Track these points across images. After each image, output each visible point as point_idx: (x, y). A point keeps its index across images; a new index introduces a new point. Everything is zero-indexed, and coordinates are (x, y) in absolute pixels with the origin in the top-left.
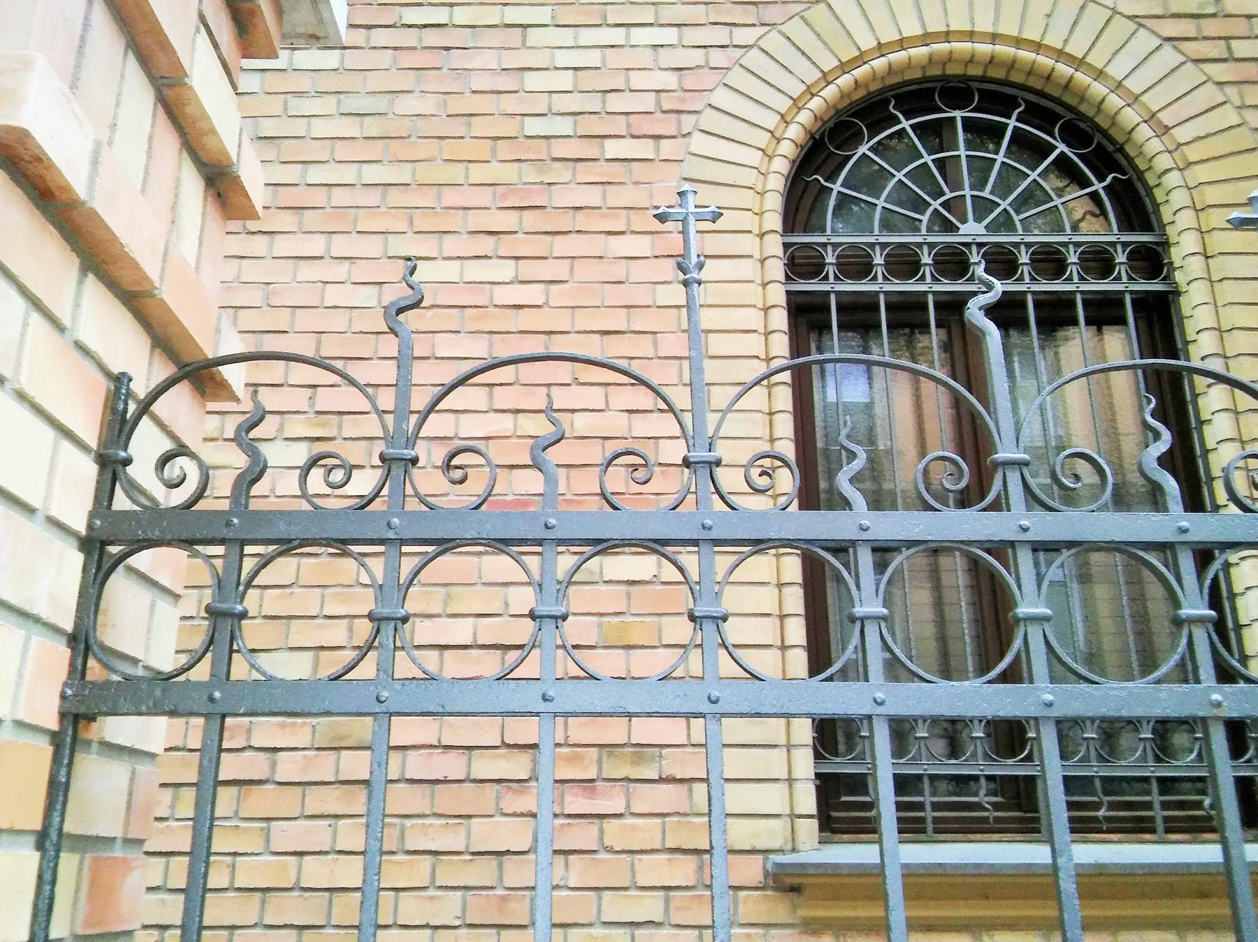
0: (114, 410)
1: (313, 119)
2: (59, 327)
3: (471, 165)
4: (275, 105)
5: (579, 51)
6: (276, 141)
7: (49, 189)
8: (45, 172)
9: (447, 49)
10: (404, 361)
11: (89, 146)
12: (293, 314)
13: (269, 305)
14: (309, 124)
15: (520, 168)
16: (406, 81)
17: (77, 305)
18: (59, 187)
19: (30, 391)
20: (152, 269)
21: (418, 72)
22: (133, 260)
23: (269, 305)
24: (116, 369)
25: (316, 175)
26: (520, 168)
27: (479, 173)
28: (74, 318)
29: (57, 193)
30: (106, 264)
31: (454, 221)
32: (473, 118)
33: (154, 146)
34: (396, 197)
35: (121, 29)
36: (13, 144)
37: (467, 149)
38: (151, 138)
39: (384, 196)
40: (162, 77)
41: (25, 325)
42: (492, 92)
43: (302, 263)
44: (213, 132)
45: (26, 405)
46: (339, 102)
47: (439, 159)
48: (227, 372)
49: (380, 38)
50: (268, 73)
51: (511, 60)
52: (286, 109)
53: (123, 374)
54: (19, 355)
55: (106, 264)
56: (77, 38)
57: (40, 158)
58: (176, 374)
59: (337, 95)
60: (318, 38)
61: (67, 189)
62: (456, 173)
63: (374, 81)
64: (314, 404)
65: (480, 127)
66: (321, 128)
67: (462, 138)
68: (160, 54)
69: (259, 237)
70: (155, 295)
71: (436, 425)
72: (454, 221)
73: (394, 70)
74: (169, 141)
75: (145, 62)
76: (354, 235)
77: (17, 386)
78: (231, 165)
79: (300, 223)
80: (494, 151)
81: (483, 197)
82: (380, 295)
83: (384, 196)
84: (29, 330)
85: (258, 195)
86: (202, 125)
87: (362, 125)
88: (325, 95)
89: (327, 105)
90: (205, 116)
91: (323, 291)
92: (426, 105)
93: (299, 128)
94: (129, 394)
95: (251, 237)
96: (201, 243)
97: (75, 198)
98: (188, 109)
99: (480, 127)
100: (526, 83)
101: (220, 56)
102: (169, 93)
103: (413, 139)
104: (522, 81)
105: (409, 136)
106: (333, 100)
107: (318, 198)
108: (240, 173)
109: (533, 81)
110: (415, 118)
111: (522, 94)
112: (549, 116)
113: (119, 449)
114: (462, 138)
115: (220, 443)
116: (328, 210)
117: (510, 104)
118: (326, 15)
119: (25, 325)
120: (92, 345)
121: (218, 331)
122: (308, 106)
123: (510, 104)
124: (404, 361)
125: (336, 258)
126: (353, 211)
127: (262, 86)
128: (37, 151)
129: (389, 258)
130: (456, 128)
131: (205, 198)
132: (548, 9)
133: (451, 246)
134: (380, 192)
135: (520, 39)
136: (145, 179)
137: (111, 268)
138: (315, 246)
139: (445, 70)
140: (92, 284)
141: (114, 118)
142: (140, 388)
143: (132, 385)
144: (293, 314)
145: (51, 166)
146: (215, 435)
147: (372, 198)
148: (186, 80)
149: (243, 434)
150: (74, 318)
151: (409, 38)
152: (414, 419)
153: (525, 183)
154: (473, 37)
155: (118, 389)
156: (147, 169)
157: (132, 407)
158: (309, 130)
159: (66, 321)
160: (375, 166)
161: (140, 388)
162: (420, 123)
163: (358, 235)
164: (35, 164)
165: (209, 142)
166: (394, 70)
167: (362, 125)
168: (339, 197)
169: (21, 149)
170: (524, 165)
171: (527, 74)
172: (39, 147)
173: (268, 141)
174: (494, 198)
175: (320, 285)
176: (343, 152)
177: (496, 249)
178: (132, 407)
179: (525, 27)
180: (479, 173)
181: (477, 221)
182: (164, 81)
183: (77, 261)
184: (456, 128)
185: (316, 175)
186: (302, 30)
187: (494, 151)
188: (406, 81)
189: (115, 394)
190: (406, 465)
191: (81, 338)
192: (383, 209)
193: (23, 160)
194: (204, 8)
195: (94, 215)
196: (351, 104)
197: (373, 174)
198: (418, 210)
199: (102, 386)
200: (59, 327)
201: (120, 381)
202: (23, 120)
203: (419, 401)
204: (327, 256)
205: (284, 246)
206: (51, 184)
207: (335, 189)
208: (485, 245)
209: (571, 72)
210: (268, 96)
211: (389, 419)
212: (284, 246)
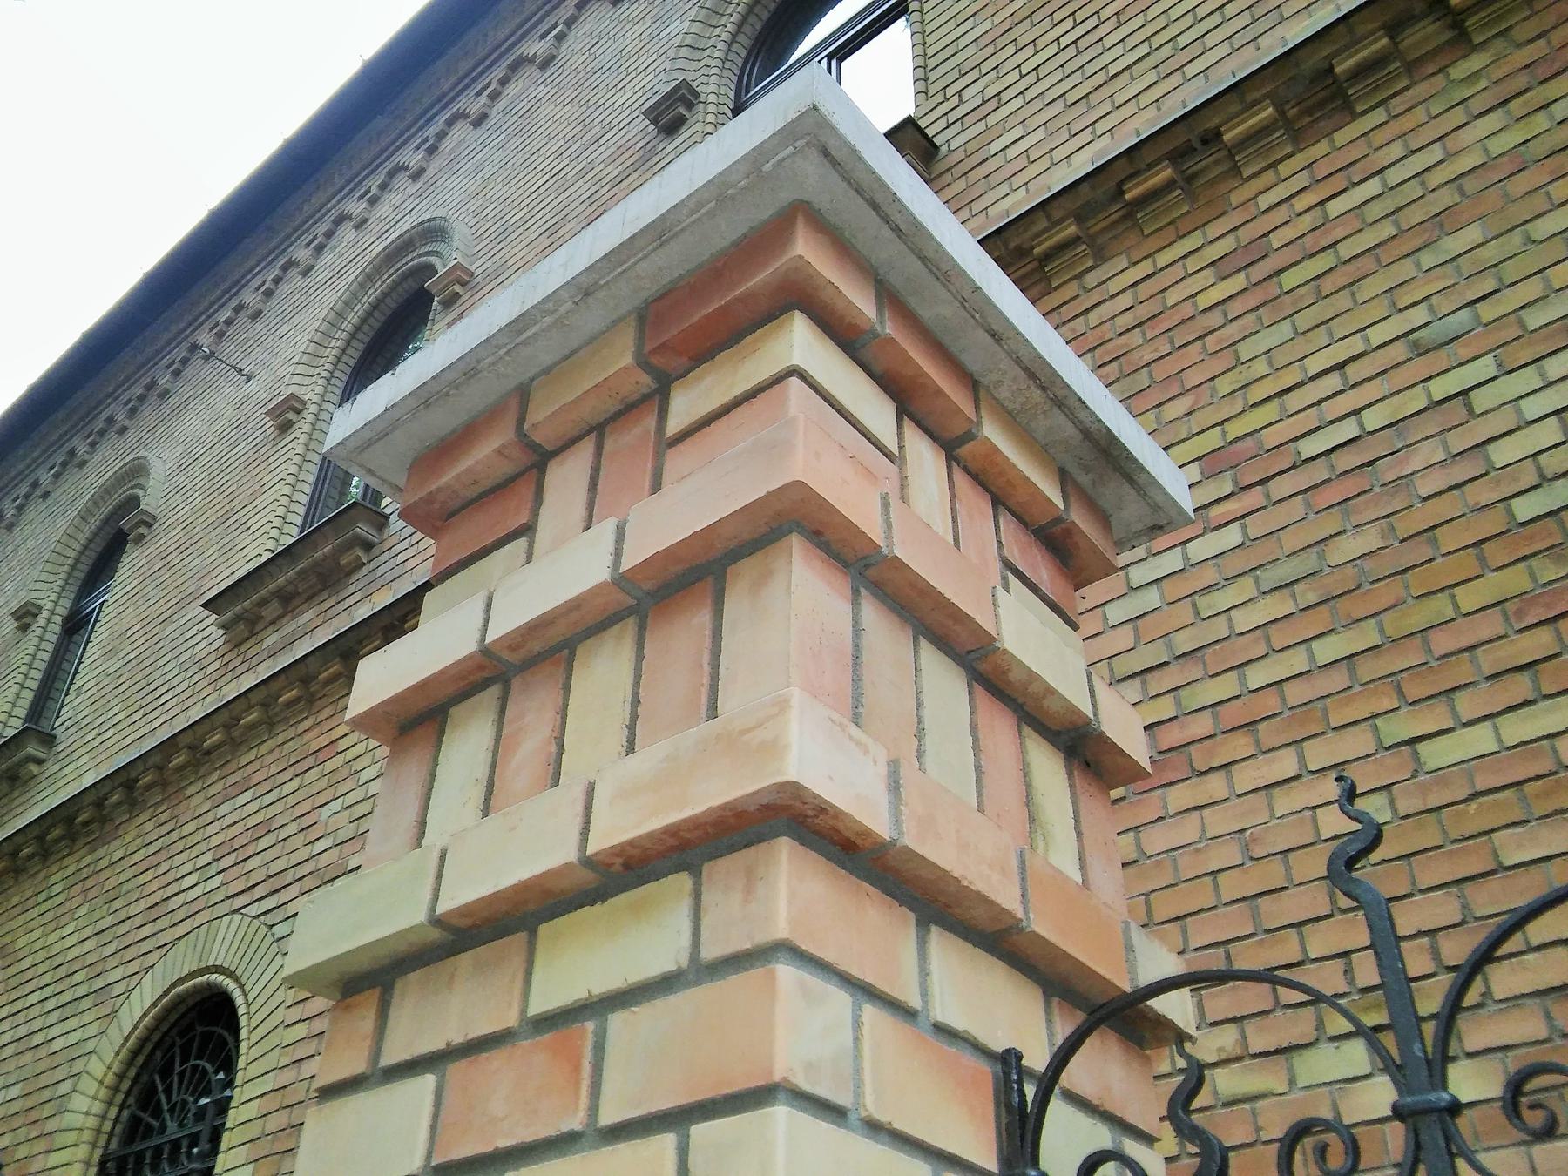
0: (1008, 1105)
1: (1233, 613)
2: (908, 1014)
3: (1456, 590)
4: (1184, 613)
5: (1555, 387)
6: (1199, 654)
7: (848, 840)
8: (835, 822)
9: (1371, 463)
10: (1386, 943)
11: (882, 770)
12: (1286, 862)
13: (1252, 859)
14: (1230, 620)
15: (1530, 567)
16: (1330, 524)
17: (924, 973)
18: (858, 834)
19: (883, 1117)
20: (1007, 897)
21: (1343, 506)
22: (978, 893)
23: (1252, 859)
24: (999, 1047)
25: (1257, 677)
26: (1530, 567)
27: (1469, 598)
28: (924, 993)
29: (859, 842)
30: (950, 907)
31: (1462, 671)
32: (1436, 531)
33: (981, 736)
34: (1369, 669)
35: (900, 616)
36: (790, 802)
37: (1445, 570)
38: (974, 729)
39: (1352, 672)
40: (969, 652)
41: (857, 1024)
42: (1451, 488)
43: (1276, 791)
44: (1051, 691)
45: (884, 1137)
46: (1257, 579)
47: (1410, 600)
48: (1161, 1004)
49: (1281, 487)
50: (1165, 581)
51: (1458, 442)
52: (1197, 613)
53: (1008, 1051)
54: (858, 1070)
55: (950, 907)
56: (849, 649)
57: (823, 808)
58: (1084, 1022)
59: (1252, 574)
60: (1161, 527)
61: (866, 833)
62: (1441, 607)
63: (1291, 541)
64: (1353, 979)
65: (1449, 539)
66: (1245, 620)
67: (1431, 560)
68: (957, 628)
69: (1212, 777)
70: (1023, 929)
71: (1474, 1033)
72: (1462, 671)
73: (1311, 516)
74: (1000, 727)
75: (943, 644)
76: (1330, 734)
77: (863, 1114)
78: (1088, 722)
79: (1258, 743)
80: (1482, 559)
81: (1490, 625)
82: (1392, 802)
83: (1352, 672)
84: (866, 1029)
85: (1137, 748)
86: (1034, 688)
87: (1294, 596)
88: (1239, 579)
89: (1246, 588)
90: (1033, 676)
91: (1314, 820)
92: (1369, 540)
93: (1220, 628)
94: (1023, 1073)
95: (1204, 778)
96: (1079, 834)
97: (879, 840)
98: (1012, 676)
99: (1449, 539)
100: (1494, 457)
101: (1044, 599)
102: (982, 667)
103: (1366, 586)
104: (1488, 459)
105: (1359, 586)
106: (1248, 581)
107: (1271, 703)
108: (1104, 728)
109: (1502, 453)
110: (1358, 562)
111: (1493, 474)
112: (1545, 485)
113: (1025, 1167)
114: (1431, 560)
115: (1247, 1062)
116: (1287, 713)
117: (1482, 493)
118: (1159, 498)
119: (857, 1024)
120: (958, 1023)
121: (1129, 948)
122: (1223, 599)
123: (1482, 493)
124: (1386, 943)
125: (1317, 771)
126: (1319, 705)
127: (1162, 596)
128: (816, 802)
129: (1387, 749)
130: (1421, 552)
131: (1070, 774)
132: (1489, 359)
133: (1467, 705)
134: (1344, 670)
135: (1464, 411)
136: (978, 779)
137: (957, 911)
138: (1286, 764)
139: (1377, 489)
140: (938, 939)
141: (919, 723)
142: (1037, 1059)
143: (1024, 1062)
144: (1286, 862)
145: (838, 814)
146: (1238, 1052)
147: (1338, 679)
148: (997, 644)
149: (1180, 1111)
150: (924, 993)
151: (1319, 472)
152: (1429, 1029)
153: (1545, 585)
154: (1399, 436)
155: (1007, 1075)
156: (978, 768)
157: (1030, 1090)
158: (1231, 627)
159: (915, 1002)
160: (1328, 639)
161: (1037, 1059)
162: (1368, 564)
163: (1335, 733)
164: (821, 817)
165: (1050, 704)
166: (1311, 516)
167: (1294, 596)
168: (1297, 693)
169: (798, 804)
170: (1534, 562)
171: (1491, 448)
172: (816, 796)
173: (1188, 657)
174: (1507, 619)
175: (1307, 813)
176: (1279, 638)
177: (1537, 688)
178: (1030, 1090)
179: (1464, 393)
180: (1469, 598)
181: (1489, 661)
182: (973, 656)
183: (912, 916)
184: (1421, 552)
185: (1257, 677)
186: (1140, 527)
187: (1482, 559)
188: (1330, 524)
189: (1005, 1083)
190: (1442, 1122)
191: (940, 1019)
192: (1357, 688)
193: (806, 816)
194: (1006, 553)
195: (908, 851)
196: (1271, 577)
197: (1326, 650)
198: (1404, 675)
199: (986, 1072)
200: (908, 1014)
201: (1009, 1061)
202: (791, 773)
203: (1430, 1000)
204: (1304, 773)
205: (1246, 778)
206: (847, 834)
207: (1287, 686)
208: (1521, 686)
209: (1553, 419)
210: (1172, 606)
211: (1388, 1040)
212: (1246, 778)
